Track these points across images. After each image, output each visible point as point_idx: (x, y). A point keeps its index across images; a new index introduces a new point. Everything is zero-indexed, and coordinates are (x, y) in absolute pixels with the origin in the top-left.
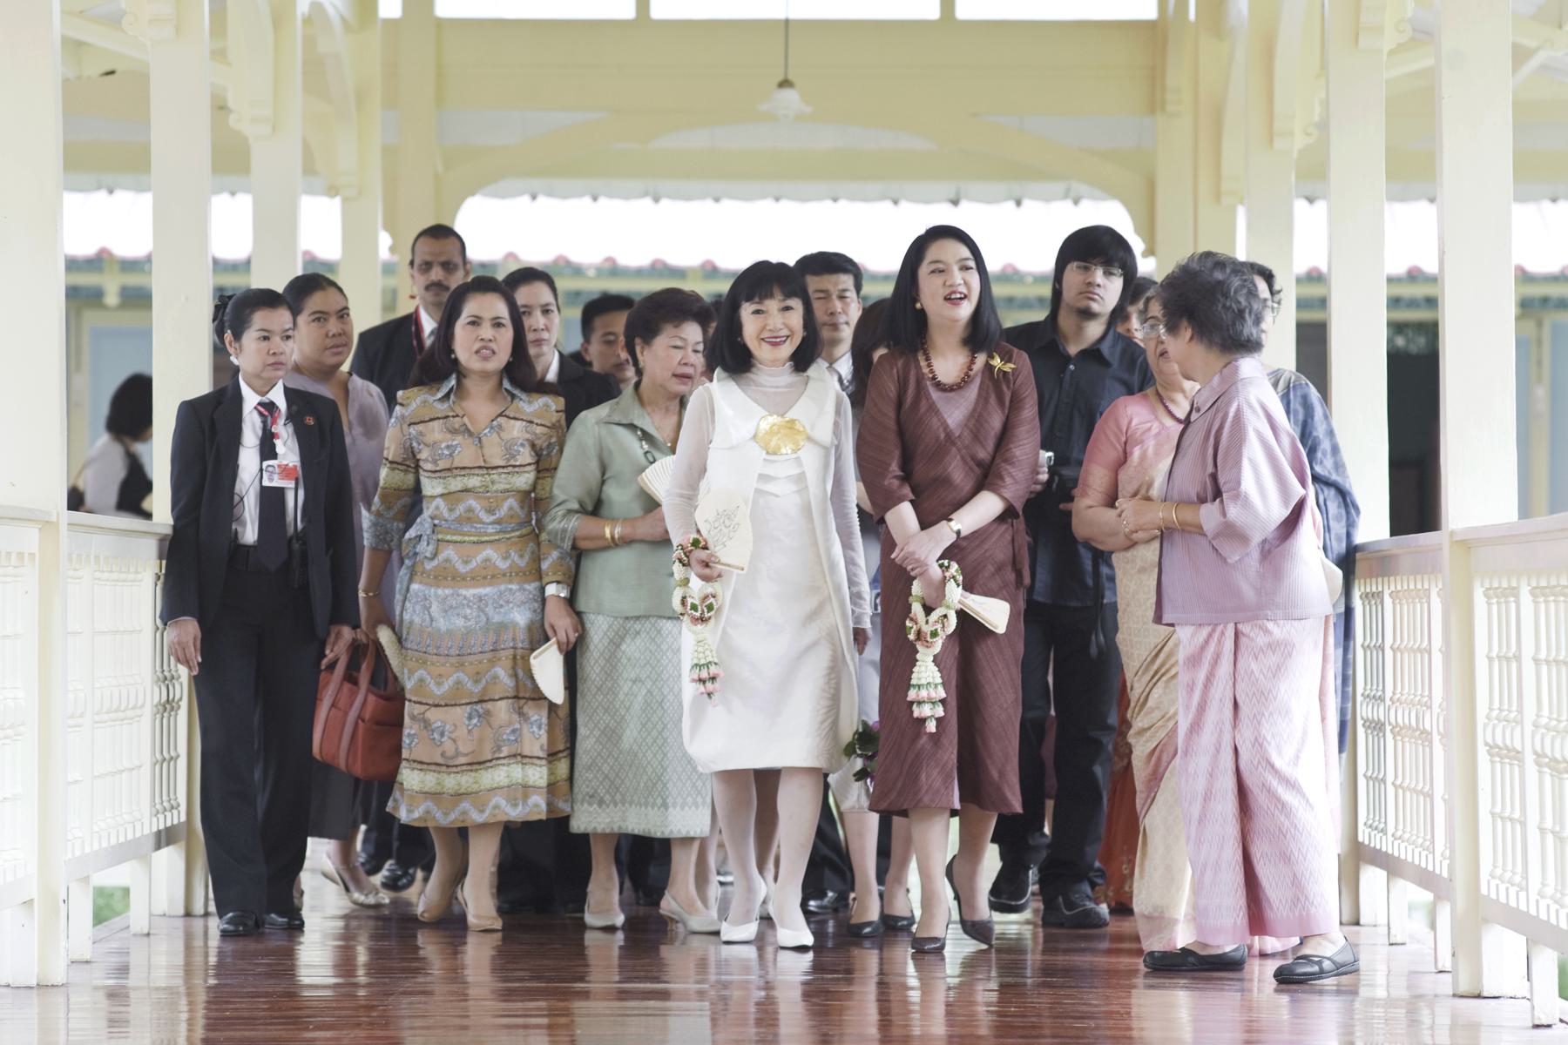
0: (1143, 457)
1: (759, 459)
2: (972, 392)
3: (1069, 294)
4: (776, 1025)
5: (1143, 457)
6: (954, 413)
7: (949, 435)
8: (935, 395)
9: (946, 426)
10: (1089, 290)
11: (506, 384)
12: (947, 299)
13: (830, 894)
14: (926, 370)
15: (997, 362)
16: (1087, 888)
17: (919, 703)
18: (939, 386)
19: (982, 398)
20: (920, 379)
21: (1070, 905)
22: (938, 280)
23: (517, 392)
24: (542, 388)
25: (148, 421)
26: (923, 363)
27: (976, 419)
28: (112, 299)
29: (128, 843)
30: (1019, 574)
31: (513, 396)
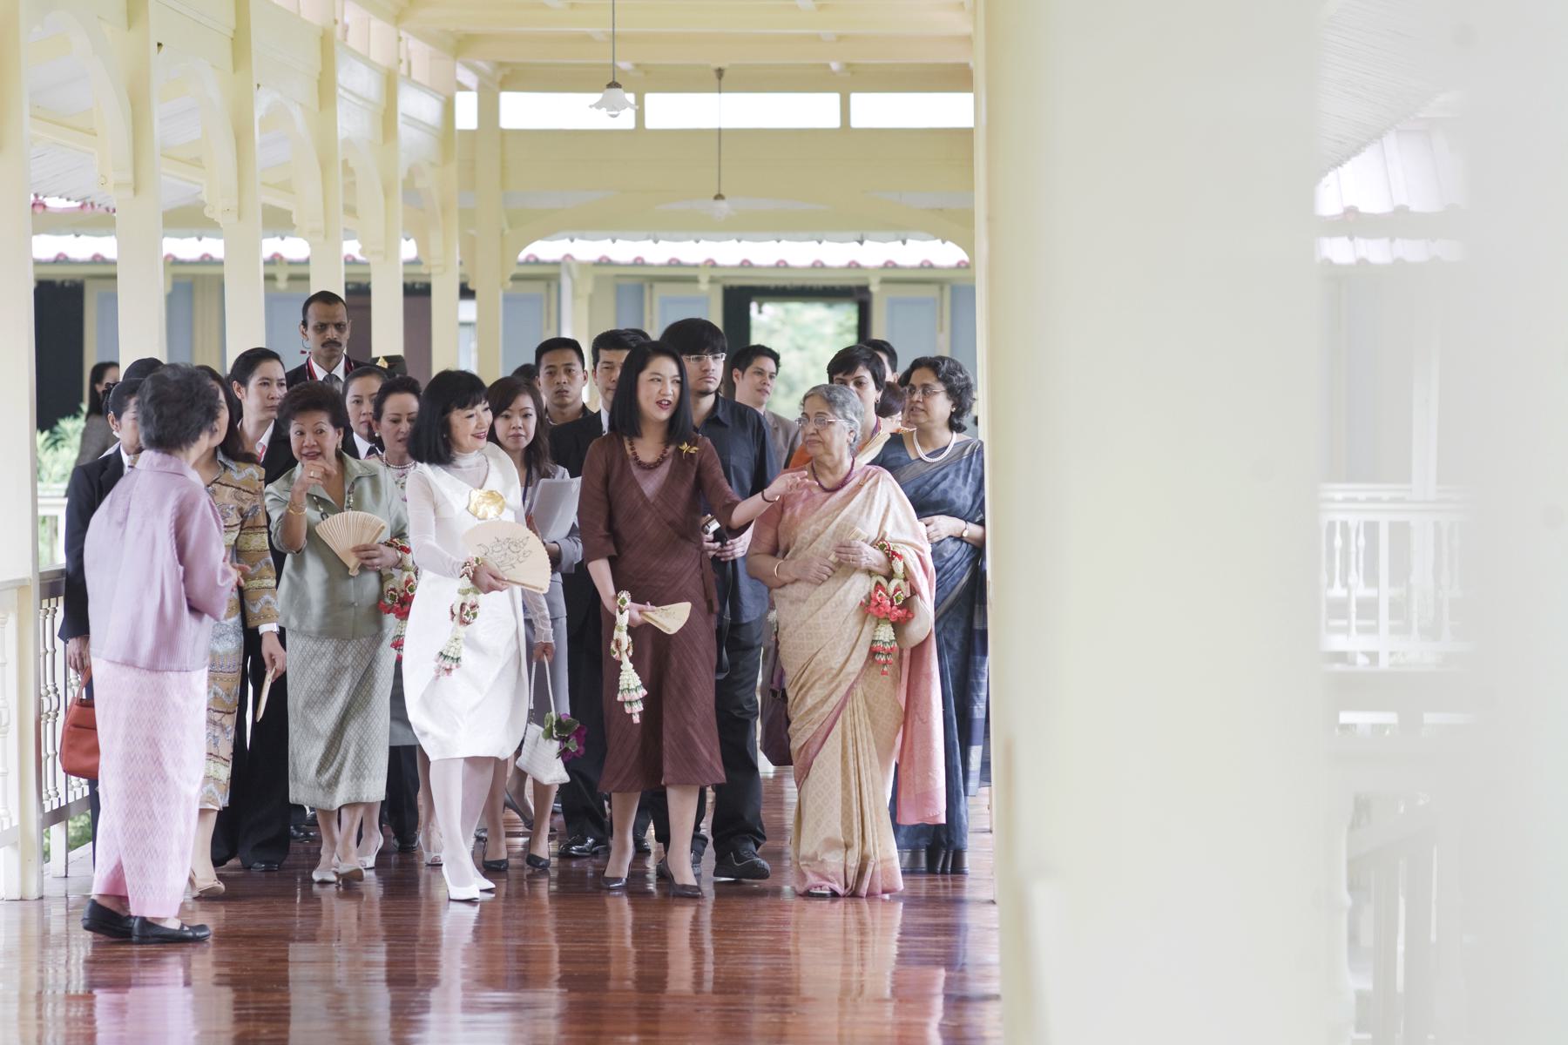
0: (792, 517)
1: (476, 516)
2: (664, 470)
3: (691, 380)
4: (287, 1022)
5: (792, 517)
6: (650, 486)
7: (646, 501)
8: (636, 472)
9: (642, 494)
10: (705, 373)
11: (221, 457)
12: (659, 403)
13: (590, 841)
14: (629, 452)
15: (685, 447)
16: (752, 846)
17: (630, 703)
18: (641, 465)
19: (672, 475)
20: (624, 459)
21: (739, 859)
22: (656, 387)
23: (229, 463)
24: (249, 458)
25: (1390, 604)
26: (628, 447)
27: (666, 489)
28: (1370, 593)
29: (53, 811)
30: (710, 603)
31: (226, 467)
